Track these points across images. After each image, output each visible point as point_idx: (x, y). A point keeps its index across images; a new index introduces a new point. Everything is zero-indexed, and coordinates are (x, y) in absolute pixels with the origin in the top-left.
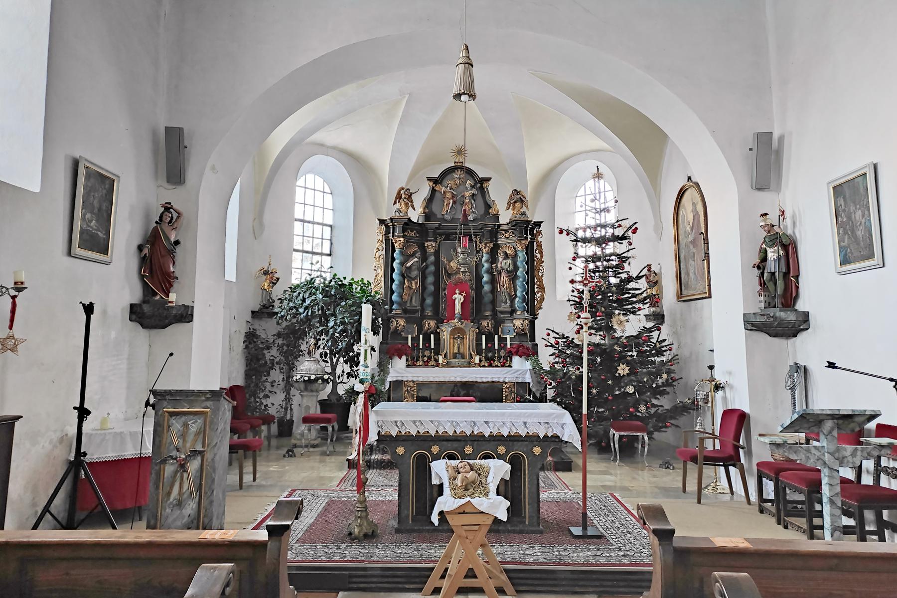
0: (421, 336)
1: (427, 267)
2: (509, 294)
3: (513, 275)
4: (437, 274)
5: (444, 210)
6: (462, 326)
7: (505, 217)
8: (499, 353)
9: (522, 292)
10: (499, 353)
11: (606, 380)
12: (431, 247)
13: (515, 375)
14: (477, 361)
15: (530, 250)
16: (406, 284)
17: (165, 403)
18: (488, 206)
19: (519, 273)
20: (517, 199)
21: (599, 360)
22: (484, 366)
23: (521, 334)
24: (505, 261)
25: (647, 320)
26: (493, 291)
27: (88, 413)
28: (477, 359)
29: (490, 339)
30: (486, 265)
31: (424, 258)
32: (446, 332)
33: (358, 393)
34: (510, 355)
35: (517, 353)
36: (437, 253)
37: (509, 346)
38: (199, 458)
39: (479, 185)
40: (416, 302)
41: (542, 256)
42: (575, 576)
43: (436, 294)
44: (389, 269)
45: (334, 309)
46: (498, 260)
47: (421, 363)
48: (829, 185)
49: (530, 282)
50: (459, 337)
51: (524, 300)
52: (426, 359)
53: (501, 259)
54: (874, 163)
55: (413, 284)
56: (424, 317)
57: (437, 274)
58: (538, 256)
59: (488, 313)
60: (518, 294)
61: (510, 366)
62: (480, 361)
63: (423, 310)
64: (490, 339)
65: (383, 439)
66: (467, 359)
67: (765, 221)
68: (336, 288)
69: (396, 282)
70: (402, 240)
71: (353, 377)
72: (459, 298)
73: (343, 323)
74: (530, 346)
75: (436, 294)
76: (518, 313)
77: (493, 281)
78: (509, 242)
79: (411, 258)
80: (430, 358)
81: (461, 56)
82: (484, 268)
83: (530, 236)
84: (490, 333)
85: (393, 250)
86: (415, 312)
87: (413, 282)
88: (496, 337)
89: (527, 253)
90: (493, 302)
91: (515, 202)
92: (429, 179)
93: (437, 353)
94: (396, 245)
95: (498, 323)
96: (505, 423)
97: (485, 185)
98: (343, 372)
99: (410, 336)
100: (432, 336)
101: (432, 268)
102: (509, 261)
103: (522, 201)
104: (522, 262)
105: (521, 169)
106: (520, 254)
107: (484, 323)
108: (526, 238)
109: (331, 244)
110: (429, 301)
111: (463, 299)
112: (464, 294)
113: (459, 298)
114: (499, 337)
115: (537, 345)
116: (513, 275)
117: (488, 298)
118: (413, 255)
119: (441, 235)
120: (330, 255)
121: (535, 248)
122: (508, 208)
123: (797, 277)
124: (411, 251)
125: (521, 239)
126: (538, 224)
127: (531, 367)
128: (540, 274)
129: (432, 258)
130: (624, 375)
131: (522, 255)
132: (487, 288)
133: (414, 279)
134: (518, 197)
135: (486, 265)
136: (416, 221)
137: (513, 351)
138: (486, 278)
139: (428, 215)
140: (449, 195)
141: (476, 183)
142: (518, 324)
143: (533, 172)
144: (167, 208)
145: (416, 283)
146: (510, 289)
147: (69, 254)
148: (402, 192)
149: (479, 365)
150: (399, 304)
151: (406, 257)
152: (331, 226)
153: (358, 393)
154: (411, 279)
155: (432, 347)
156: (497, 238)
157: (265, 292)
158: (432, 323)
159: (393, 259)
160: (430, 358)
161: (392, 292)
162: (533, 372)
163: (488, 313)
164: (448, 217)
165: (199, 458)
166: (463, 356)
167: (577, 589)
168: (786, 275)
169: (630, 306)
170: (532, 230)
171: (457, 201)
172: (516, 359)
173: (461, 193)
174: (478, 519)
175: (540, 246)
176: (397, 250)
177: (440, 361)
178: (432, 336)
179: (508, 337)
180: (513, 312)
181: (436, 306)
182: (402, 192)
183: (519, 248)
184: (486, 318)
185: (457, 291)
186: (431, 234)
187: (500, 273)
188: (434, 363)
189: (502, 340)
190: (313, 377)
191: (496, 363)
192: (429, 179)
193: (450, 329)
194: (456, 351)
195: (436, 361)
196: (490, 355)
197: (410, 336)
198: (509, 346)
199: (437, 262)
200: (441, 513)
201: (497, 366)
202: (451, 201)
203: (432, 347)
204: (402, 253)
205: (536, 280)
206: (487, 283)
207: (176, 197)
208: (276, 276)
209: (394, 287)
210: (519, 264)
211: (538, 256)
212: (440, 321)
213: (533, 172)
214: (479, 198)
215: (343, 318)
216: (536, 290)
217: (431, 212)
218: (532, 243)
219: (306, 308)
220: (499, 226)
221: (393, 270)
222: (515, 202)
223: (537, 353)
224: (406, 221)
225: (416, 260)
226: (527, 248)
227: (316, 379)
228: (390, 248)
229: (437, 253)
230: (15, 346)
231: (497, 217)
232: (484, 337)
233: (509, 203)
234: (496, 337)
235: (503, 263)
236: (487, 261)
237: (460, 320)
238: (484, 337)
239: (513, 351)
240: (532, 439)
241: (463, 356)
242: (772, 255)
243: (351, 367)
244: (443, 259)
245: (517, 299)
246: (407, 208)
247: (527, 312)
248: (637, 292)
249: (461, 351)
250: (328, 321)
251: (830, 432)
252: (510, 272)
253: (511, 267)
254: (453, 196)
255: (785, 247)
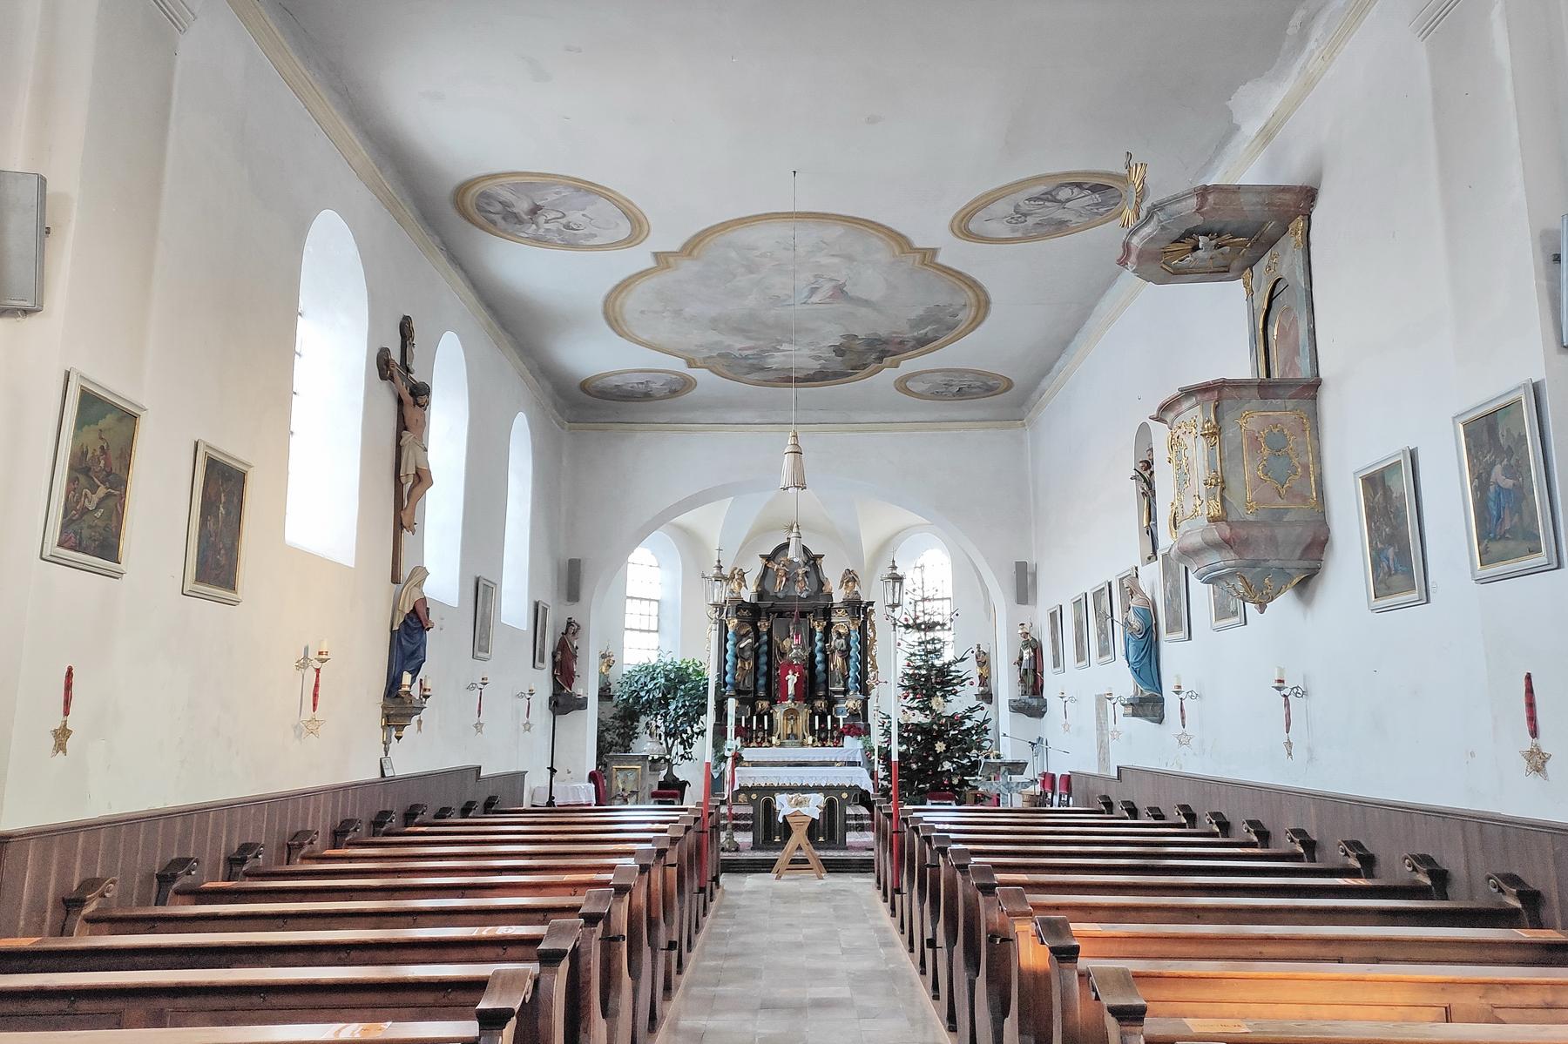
0: (755, 718)
1: (760, 646)
2: (842, 674)
3: (846, 656)
4: (769, 653)
5: (778, 587)
6: (795, 707)
7: (839, 596)
8: (832, 733)
9: (855, 672)
10: (832, 733)
11: (927, 757)
12: (763, 626)
13: (846, 754)
14: (810, 742)
15: (862, 630)
16: (739, 665)
17: (613, 763)
18: (821, 584)
19: (851, 653)
20: (850, 578)
21: (919, 738)
22: (817, 746)
23: (854, 715)
24: (838, 641)
25: (978, 699)
26: (826, 670)
27: (556, 771)
28: (810, 739)
29: (823, 720)
30: (819, 644)
31: (757, 638)
32: (779, 713)
33: (728, 757)
34: (842, 734)
35: (848, 734)
36: (769, 632)
37: (841, 727)
38: (635, 796)
39: (812, 562)
40: (749, 683)
41: (875, 635)
42: (862, 862)
43: (768, 675)
44: (723, 650)
45: (675, 693)
46: (832, 639)
47: (755, 744)
48: (1456, 420)
49: (864, 663)
50: (792, 718)
51: (856, 680)
52: (759, 740)
53: (834, 638)
54: (1534, 381)
55: (747, 665)
56: (757, 698)
57: (769, 653)
58: (872, 635)
59: (821, 693)
60: (851, 674)
61: (842, 746)
62: (814, 741)
63: (756, 691)
64: (823, 720)
65: (743, 789)
66: (800, 740)
67: (1022, 629)
68: (675, 672)
69: (729, 663)
70: (736, 621)
71: (686, 759)
72: (792, 679)
73: (683, 706)
74: (862, 728)
75: (768, 675)
76: (851, 693)
77: (826, 661)
78: (841, 621)
79: (744, 639)
80: (763, 739)
81: (789, 443)
82: (818, 647)
83: (862, 616)
84: (823, 712)
85: (727, 631)
86: (747, 692)
87: (746, 663)
88: (829, 717)
89: (859, 633)
90: (826, 682)
91: (848, 582)
92: (762, 556)
93: (771, 733)
94: (729, 626)
95: (831, 702)
96: (823, 777)
97: (818, 562)
98: (677, 754)
99: (743, 717)
100: (766, 717)
101: (765, 648)
102: (843, 641)
103: (855, 581)
104: (855, 642)
105: (856, 539)
106: (853, 634)
107: (818, 703)
108: (859, 618)
109: (659, 620)
110: (762, 681)
111: (796, 680)
112: (797, 675)
113: (792, 679)
114: (832, 717)
115: (869, 725)
116: (846, 656)
117: (821, 678)
118: (746, 635)
119: (774, 613)
120: (657, 631)
121: (868, 627)
122: (841, 587)
123: (1042, 673)
124: (743, 632)
125: (853, 619)
126: (871, 603)
127: (862, 747)
128: (874, 654)
129: (765, 638)
130: (941, 752)
131: (854, 636)
132: (820, 667)
133: (747, 660)
134: (851, 576)
135: (819, 644)
136: (748, 601)
137: (845, 731)
138: (819, 657)
139: (761, 595)
140: (781, 573)
141: (809, 559)
142: (850, 704)
143: (868, 543)
144: (569, 624)
145: (749, 664)
146: (843, 668)
147: (534, 667)
148: (736, 572)
149: (812, 745)
150: (732, 685)
151: (740, 637)
152: (658, 601)
153: (728, 757)
154: (744, 660)
155: (766, 728)
156: (830, 616)
157: (602, 675)
158: (766, 704)
159: (727, 640)
160: (763, 739)
161: (726, 673)
162: (864, 751)
163: (821, 693)
164: (781, 595)
165: (635, 796)
166: (796, 737)
167: (863, 870)
168: (1035, 670)
169: (951, 688)
170: (865, 608)
171: (791, 579)
172: (847, 738)
173: (794, 569)
174: (803, 819)
175: (872, 625)
176: (731, 631)
177: (774, 742)
178: (766, 717)
179: (841, 717)
180: (846, 692)
181: (768, 686)
182: (736, 572)
183: (852, 628)
184: (819, 698)
185: (790, 672)
186: (763, 613)
187: (833, 652)
188: (767, 744)
189: (835, 721)
190: (656, 757)
191: (829, 743)
192: (762, 556)
193: (784, 710)
194: (789, 732)
195: (770, 742)
196: (823, 735)
197: (743, 717)
198: (841, 727)
199: (769, 642)
200: (784, 817)
201: (830, 746)
202: (784, 579)
203: (766, 728)
204: (735, 633)
205: (869, 659)
206: (821, 662)
207: (573, 611)
208: (612, 659)
209: (727, 668)
210: (852, 644)
211: (872, 635)
212: (773, 702)
213: (868, 543)
214: (813, 576)
215: (685, 701)
216: (869, 670)
217: (763, 588)
218: (864, 622)
219: (648, 692)
220: (832, 605)
221: (726, 651)
222: (848, 582)
223: (869, 734)
224: (740, 603)
225: (750, 641)
226: (859, 628)
227: (660, 759)
228: (723, 629)
229: (769, 632)
230: (530, 728)
231: (830, 595)
232: (817, 717)
233: (842, 581)
234: (829, 717)
235: (836, 643)
236: (820, 640)
237: (793, 701)
238: (817, 717)
239: (845, 731)
240: (842, 788)
241: (796, 737)
242: (1026, 657)
243: (685, 748)
244: (776, 638)
245: (850, 679)
246: (740, 587)
247: (860, 692)
248: (960, 674)
249: (795, 732)
250: (668, 704)
251: (1003, 774)
252: (843, 651)
253: (845, 647)
254: (786, 573)
255: (1034, 651)
